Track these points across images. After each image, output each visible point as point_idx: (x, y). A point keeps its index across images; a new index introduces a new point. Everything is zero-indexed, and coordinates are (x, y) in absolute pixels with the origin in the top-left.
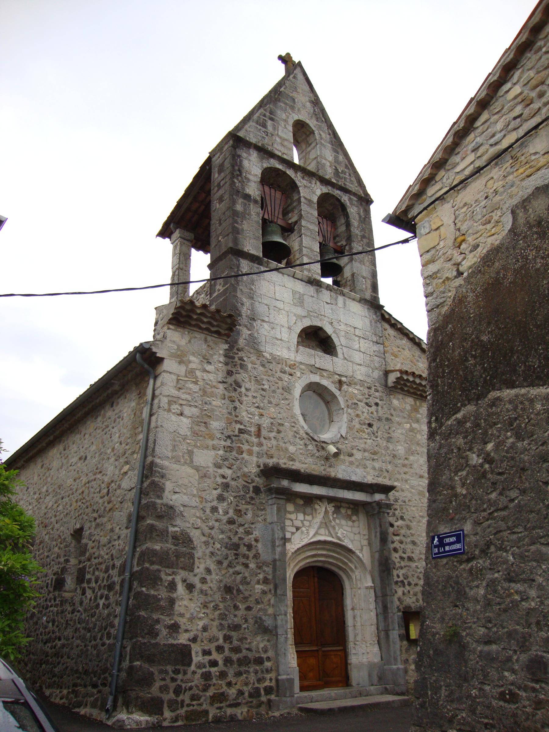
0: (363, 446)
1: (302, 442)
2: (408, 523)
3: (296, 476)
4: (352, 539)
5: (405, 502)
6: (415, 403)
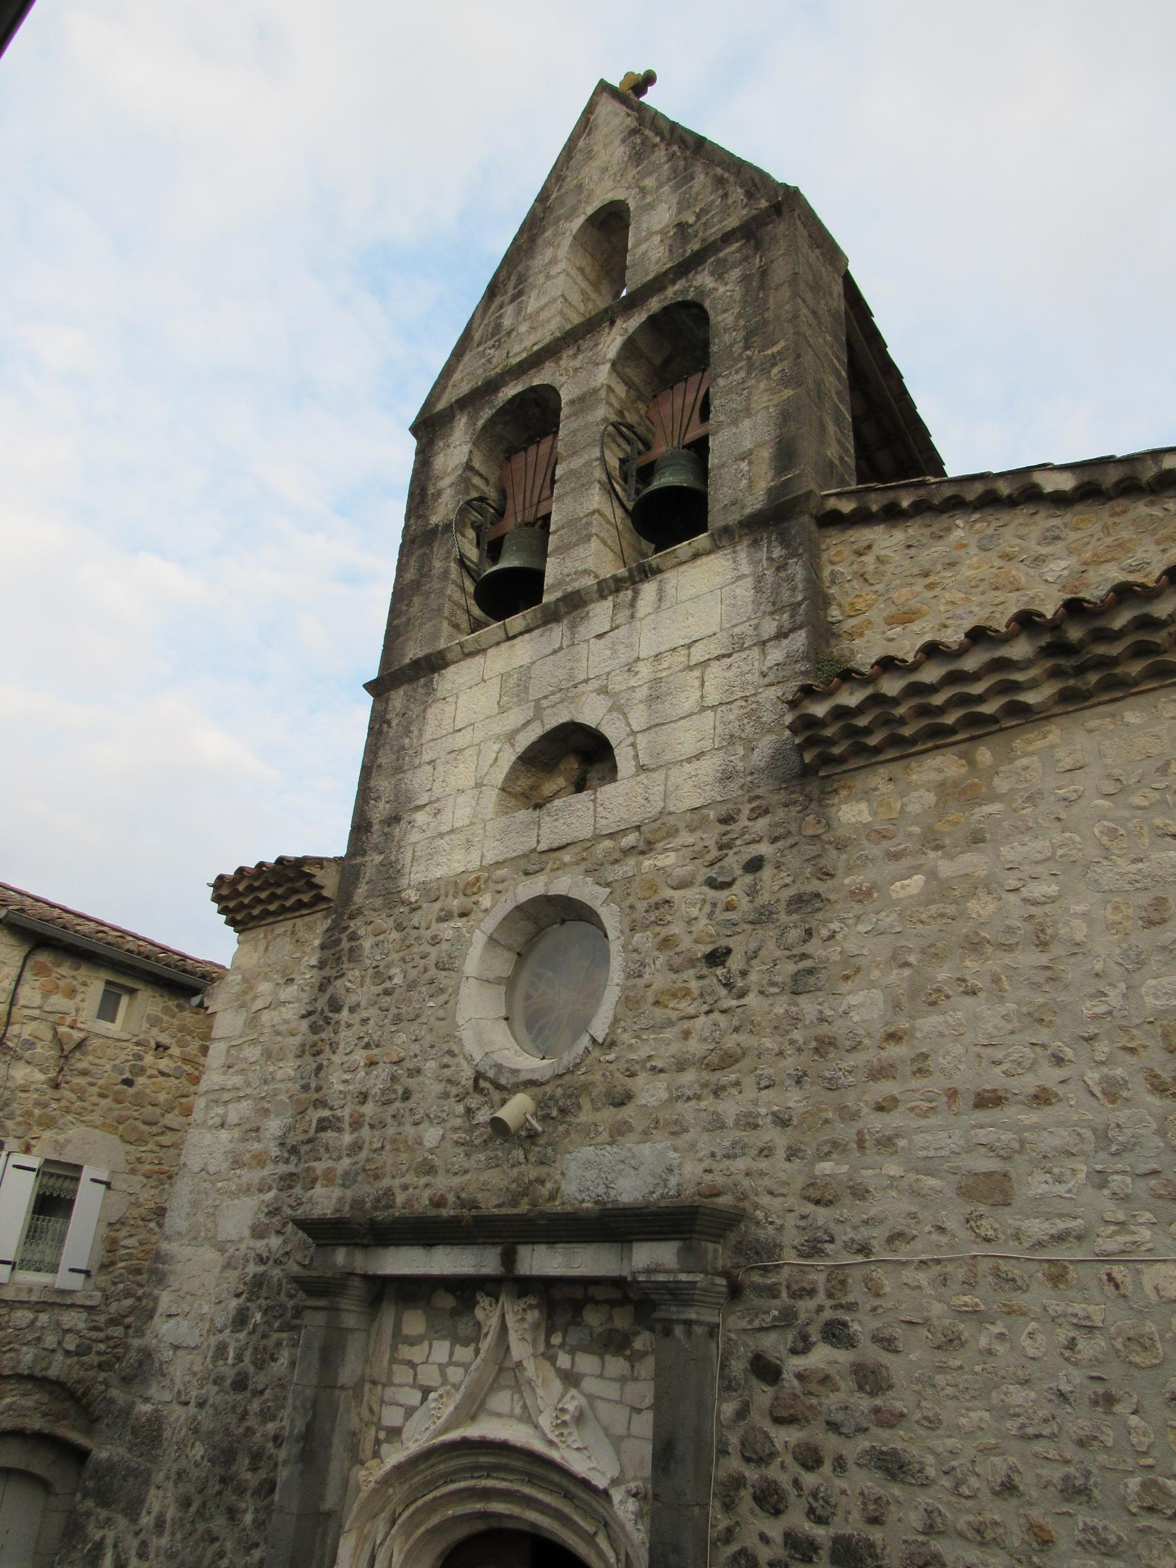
2: (871, 1353)
4: (619, 1429)
5: (865, 1249)
6: (972, 763)
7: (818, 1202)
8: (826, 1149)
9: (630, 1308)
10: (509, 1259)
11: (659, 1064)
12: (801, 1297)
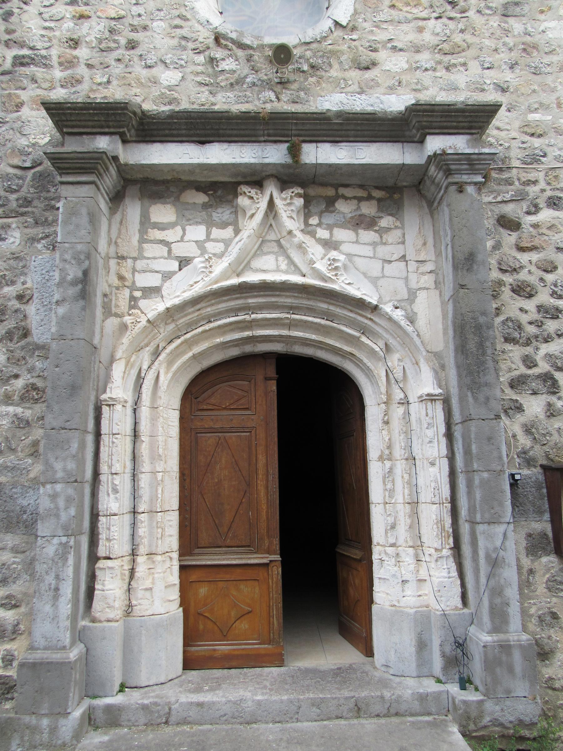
0: (412, 36)
1: (201, 59)
3: (151, 129)
7: (532, 135)
8: (536, 106)
9: (374, 202)
10: (294, 152)
11: (400, 45)
12: (528, 184)
